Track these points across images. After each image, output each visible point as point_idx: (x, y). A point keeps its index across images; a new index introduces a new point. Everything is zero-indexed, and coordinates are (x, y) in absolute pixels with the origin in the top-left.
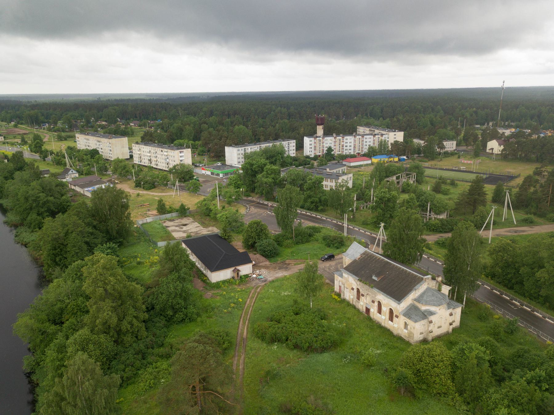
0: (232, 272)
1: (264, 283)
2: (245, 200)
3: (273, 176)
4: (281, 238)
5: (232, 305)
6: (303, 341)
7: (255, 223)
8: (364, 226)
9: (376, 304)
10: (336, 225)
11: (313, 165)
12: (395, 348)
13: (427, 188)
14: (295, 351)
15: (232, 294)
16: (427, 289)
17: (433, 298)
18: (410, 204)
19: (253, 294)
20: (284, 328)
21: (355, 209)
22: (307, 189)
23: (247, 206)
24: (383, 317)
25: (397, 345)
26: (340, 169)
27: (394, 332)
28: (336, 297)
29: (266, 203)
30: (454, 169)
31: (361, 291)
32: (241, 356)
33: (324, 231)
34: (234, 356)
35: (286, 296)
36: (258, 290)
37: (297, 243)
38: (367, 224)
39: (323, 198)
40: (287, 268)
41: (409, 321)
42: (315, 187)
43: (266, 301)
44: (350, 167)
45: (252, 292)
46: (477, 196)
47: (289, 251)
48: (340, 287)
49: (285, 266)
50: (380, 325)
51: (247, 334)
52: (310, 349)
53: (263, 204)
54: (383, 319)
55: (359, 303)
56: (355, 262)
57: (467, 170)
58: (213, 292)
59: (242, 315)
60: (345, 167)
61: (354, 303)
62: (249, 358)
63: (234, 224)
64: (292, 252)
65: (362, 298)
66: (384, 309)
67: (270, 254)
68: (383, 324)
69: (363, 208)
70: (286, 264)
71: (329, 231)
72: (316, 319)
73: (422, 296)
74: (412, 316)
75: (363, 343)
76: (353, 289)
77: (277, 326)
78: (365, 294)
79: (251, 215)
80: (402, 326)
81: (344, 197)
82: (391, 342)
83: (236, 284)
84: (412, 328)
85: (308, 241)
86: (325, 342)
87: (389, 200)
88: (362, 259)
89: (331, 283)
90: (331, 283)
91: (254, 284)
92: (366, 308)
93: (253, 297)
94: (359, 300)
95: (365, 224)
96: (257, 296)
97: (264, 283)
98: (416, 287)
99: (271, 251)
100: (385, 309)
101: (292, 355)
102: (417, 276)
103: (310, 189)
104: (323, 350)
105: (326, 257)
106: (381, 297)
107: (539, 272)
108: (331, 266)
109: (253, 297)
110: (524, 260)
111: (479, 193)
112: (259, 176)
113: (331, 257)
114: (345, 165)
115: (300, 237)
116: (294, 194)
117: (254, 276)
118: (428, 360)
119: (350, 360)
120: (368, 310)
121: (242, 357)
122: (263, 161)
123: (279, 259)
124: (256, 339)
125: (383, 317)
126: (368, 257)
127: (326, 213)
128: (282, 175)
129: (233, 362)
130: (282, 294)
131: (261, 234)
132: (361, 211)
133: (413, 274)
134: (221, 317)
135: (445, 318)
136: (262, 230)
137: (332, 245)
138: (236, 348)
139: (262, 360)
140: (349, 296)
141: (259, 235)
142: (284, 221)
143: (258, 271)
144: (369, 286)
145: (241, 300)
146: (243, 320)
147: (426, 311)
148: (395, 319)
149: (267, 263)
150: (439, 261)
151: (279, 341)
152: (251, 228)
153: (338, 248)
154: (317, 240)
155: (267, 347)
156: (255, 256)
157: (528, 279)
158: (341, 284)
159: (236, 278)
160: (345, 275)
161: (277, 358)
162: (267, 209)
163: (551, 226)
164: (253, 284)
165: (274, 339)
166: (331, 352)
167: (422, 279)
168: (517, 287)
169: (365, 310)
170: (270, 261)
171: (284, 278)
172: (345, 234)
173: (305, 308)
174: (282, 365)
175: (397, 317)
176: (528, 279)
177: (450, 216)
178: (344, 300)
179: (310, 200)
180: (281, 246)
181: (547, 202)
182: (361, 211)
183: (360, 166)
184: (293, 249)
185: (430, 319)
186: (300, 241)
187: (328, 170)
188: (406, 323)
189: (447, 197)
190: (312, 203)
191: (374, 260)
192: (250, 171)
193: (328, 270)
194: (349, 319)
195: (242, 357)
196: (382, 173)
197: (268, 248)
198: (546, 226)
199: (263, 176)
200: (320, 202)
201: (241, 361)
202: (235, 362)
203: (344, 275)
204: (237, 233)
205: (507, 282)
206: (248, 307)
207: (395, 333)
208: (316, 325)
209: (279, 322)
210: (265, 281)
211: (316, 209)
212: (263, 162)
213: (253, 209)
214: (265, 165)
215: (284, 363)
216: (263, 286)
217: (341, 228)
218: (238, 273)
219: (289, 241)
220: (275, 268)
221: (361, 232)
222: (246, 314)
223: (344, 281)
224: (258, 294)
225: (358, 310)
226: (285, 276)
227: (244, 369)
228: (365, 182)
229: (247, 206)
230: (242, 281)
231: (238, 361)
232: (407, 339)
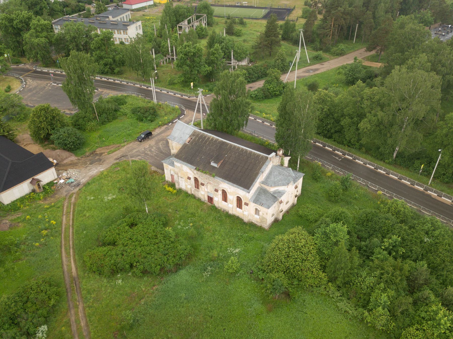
0: (30, 185)
1: (78, 189)
2: (15, 69)
3: (45, 34)
4: (81, 121)
5: (44, 232)
6: (153, 265)
7: (41, 110)
8: (171, 86)
9: (220, 192)
10: (141, 91)
11: (89, 11)
12: (251, 239)
13: (220, 30)
14: (145, 279)
15: (40, 216)
16: (272, 168)
17: (280, 177)
18: (216, 55)
19: (67, 207)
20: (124, 253)
21: (155, 66)
22: (95, 48)
23: (21, 77)
24: (230, 206)
25: (251, 234)
26: (124, 15)
27: (244, 219)
28: (171, 189)
29: (45, 70)
30: (237, 4)
31: (199, 180)
32: (77, 307)
33: (129, 101)
34: (69, 310)
35: (111, 200)
36: (73, 199)
37: (103, 123)
38: (174, 84)
39: (117, 58)
40: (100, 160)
41: (259, 208)
42: (104, 45)
43: (87, 215)
44: (132, 10)
45: (66, 204)
46: (274, 38)
47: (95, 135)
48: (172, 176)
49: (97, 157)
50: (227, 213)
51: (77, 269)
52: (164, 271)
53: (41, 73)
54: (230, 207)
55: (198, 191)
56: (185, 146)
57: (249, 5)
58: (11, 218)
59: (61, 241)
60: (129, 13)
61: (193, 192)
62: (89, 307)
63: (11, 110)
64: (100, 137)
65: (201, 187)
66: (229, 197)
67: (74, 146)
68: (231, 212)
69: (163, 63)
70: (97, 154)
71: (136, 100)
72: (159, 229)
73: (268, 177)
74: (263, 202)
75: (217, 242)
76: (189, 178)
77: (113, 252)
78: (205, 183)
79: (30, 90)
80: (253, 212)
81: (142, 55)
82: (245, 233)
83: (40, 199)
84: (265, 214)
85: (115, 118)
86: (177, 257)
87: (194, 55)
88: (192, 143)
89: (159, 170)
90: (159, 170)
91: (65, 194)
92: (208, 197)
93: (68, 213)
94: (198, 188)
95: (171, 84)
96: (74, 209)
97: (78, 189)
98: (262, 169)
99: (73, 143)
100: (232, 198)
101: (143, 285)
102: (260, 155)
103: (99, 48)
104: (178, 267)
105: (143, 136)
106: (225, 185)
107: (362, 123)
108: (151, 147)
109: (68, 213)
110: (345, 110)
111: (275, 34)
112: (26, 36)
113: (149, 135)
114: (128, 10)
115: (104, 115)
116: (85, 63)
117: (62, 181)
118: (296, 254)
119: (211, 270)
120: (210, 199)
121: (81, 307)
122: (25, 13)
123: (87, 150)
124: (91, 275)
125: (230, 206)
126: (199, 139)
127: (125, 76)
128: (57, 30)
129: (69, 320)
130: (106, 200)
131: (54, 122)
132: (162, 67)
133: (255, 154)
134: (34, 255)
135: (290, 192)
136: (54, 117)
137: (144, 119)
138: (67, 295)
139: (107, 305)
140: (186, 185)
141: (51, 124)
142: (79, 97)
143: (64, 174)
144: (210, 175)
145: (54, 223)
146: (66, 249)
147: (275, 192)
148: (244, 206)
149: (73, 158)
150: (259, 119)
151: (121, 270)
152: (39, 117)
153: (152, 121)
154: (125, 115)
155: (108, 282)
156: (54, 153)
157: (349, 129)
158: (172, 173)
159: (38, 190)
160: (178, 164)
161: (126, 295)
162: (49, 79)
163: (336, 60)
164: (64, 193)
165: (115, 271)
166: (187, 267)
167: (267, 158)
168: (336, 136)
169: (206, 199)
170: (76, 155)
171: (101, 176)
172: (155, 101)
173: (141, 215)
174: (134, 304)
175: (246, 204)
176: (349, 129)
177: (251, 61)
178: (180, 191)
179: (102, 62)
180: (84, 130)
181: (330, 36)
182: (162, 67)
183: (144, 8)
184: (100, 132)
185: (280, 200)
186: (106, 120)
187: (111, 17)
188: (256, 209)
189: (241, 39)
190: (106, 65)
191: (206, 142)
192: (10, 29)
193: (149, 153)
194: (193, 215)
195: (81, 307)
196: (172, 18)
197: (69, 140)
198: (332, 61)
199: (31, 35)
200: (116, 62)
201: (81, 315)
202: (73, 318)
203: (175, 163)
204: (19, 121)
205: (326, 132)
206: (65, 228)
207: (246, 220)
208: (160, 237)
209: (114, 244)
210: (78, 185)
211: (112, 72)
212: (26, 16)
213: (29, 81)
214: (30, 19)
215: (137, 300)
216: (78, 194)
217: (148, 94)
218: (39, 185)
219: (93, 123)
220: (85, 163)
221: (170, 95)
222: (67, 238)
223: (176, 170)
224: (74, 206)
225: (199, 200)
226: (102, 173)
227: (87, 325)
228: (157, 30)
229: (21, 77)
230: (47, 193)
231: (76, 314)
232: (259, 224)
